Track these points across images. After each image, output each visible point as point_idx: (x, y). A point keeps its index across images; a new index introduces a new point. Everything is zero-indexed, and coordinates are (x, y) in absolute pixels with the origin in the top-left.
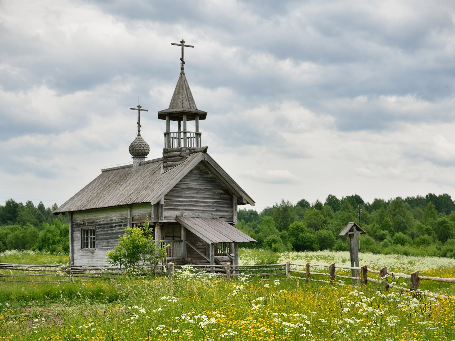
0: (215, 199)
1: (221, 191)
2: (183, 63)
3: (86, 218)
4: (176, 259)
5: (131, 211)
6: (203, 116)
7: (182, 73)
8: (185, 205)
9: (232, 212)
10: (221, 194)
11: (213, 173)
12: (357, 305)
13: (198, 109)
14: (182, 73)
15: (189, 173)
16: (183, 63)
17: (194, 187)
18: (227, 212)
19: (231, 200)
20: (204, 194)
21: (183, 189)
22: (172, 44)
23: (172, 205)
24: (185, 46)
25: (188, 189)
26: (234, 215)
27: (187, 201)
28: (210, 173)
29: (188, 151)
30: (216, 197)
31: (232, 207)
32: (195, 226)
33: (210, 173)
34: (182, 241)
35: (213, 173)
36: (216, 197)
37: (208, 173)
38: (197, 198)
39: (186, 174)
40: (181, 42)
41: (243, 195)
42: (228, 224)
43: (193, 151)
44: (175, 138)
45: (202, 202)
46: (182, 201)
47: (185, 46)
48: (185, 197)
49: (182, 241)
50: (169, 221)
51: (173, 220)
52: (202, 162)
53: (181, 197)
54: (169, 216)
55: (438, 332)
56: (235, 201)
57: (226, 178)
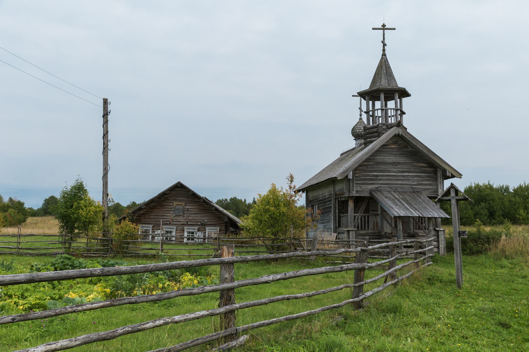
0: (416, 173)
1: (424, 165)
2: (384, 45)
3: (314, 195)
4: (371, 233)
5: (334, 187)
6: (404, 93)
7: (384, 55)
8: (381, 180)
9: (437, 185)
10: (423, 167)
11: (412, 147)
12: (166, 285)
13: (399, 86)
14: (384, 55)
15: (380, 148)
16: (384, 45)
17: (390, 161)
18: (430, 185)
19: (435, 173)
20: (403, 168)
21: (378, 163)
22: (373, 29)
23: (365, 180)
24: (387, 29)
25: (385, 163)
26: (439, 188)
27: (382, 176)
28: (409, 147)
29: (384, 127)
30: (417, 170)
31: (436, 180)
32: (386, 199)
33: (409, 147)
34: (378, 215)
35: (412, 147)
36: (417, 170)
37: (407, 148)
38: (394, 172)
39: (377, 147)
40: (382, 26)
41: (446, 167)
42: (428, 199)
43: (389, 126)
44: (393, 116)
45: (400, 176)
46: (377, 176)
47: (387, 29)
48: (381, 171)
49: (378, 215)
50: (362, 195)
51: (367, 195)
52: (397, 136)
53: (376, 171)
54: (361, 189)
55: (33, 338)
56: (439, 174)
57: (425, 151)
